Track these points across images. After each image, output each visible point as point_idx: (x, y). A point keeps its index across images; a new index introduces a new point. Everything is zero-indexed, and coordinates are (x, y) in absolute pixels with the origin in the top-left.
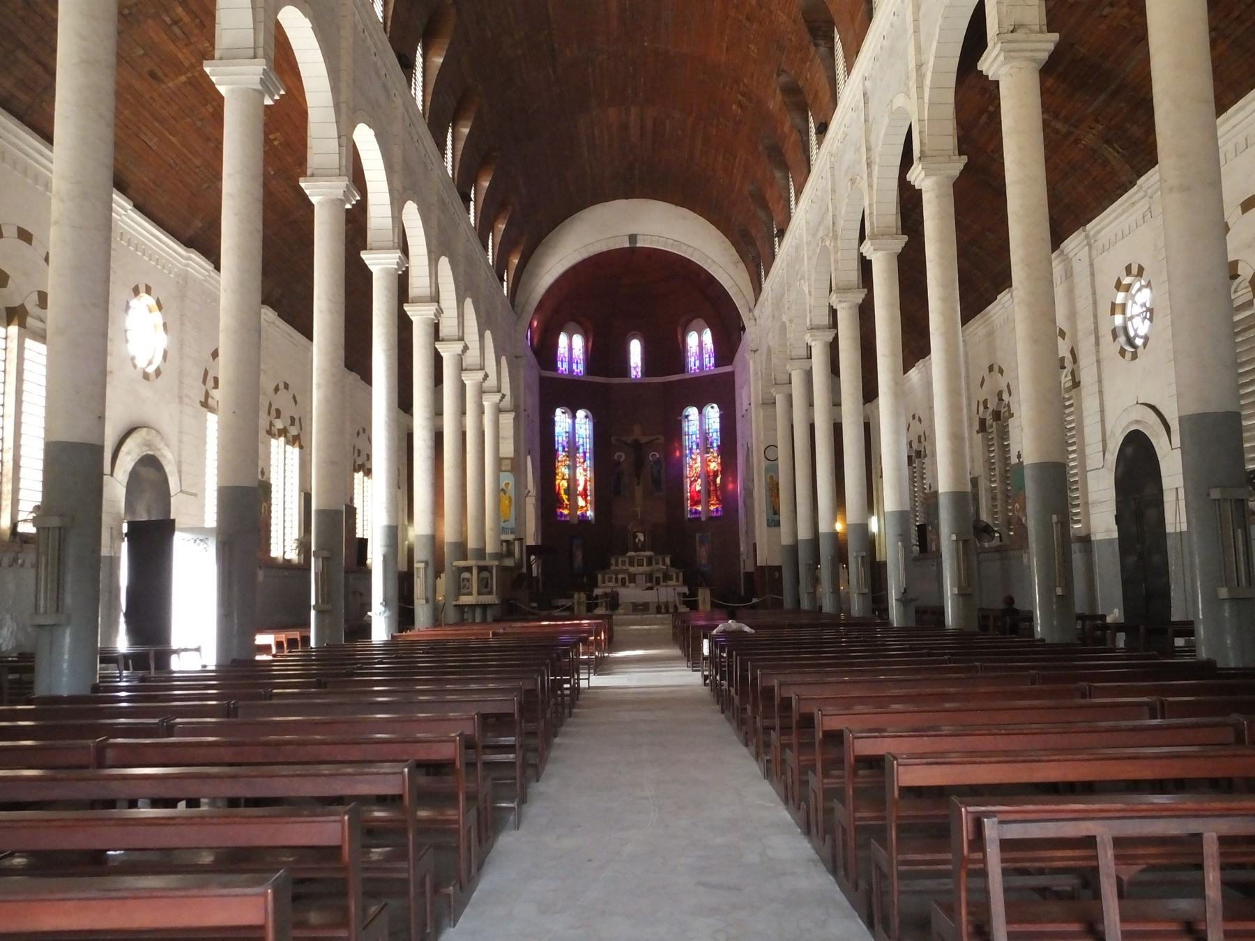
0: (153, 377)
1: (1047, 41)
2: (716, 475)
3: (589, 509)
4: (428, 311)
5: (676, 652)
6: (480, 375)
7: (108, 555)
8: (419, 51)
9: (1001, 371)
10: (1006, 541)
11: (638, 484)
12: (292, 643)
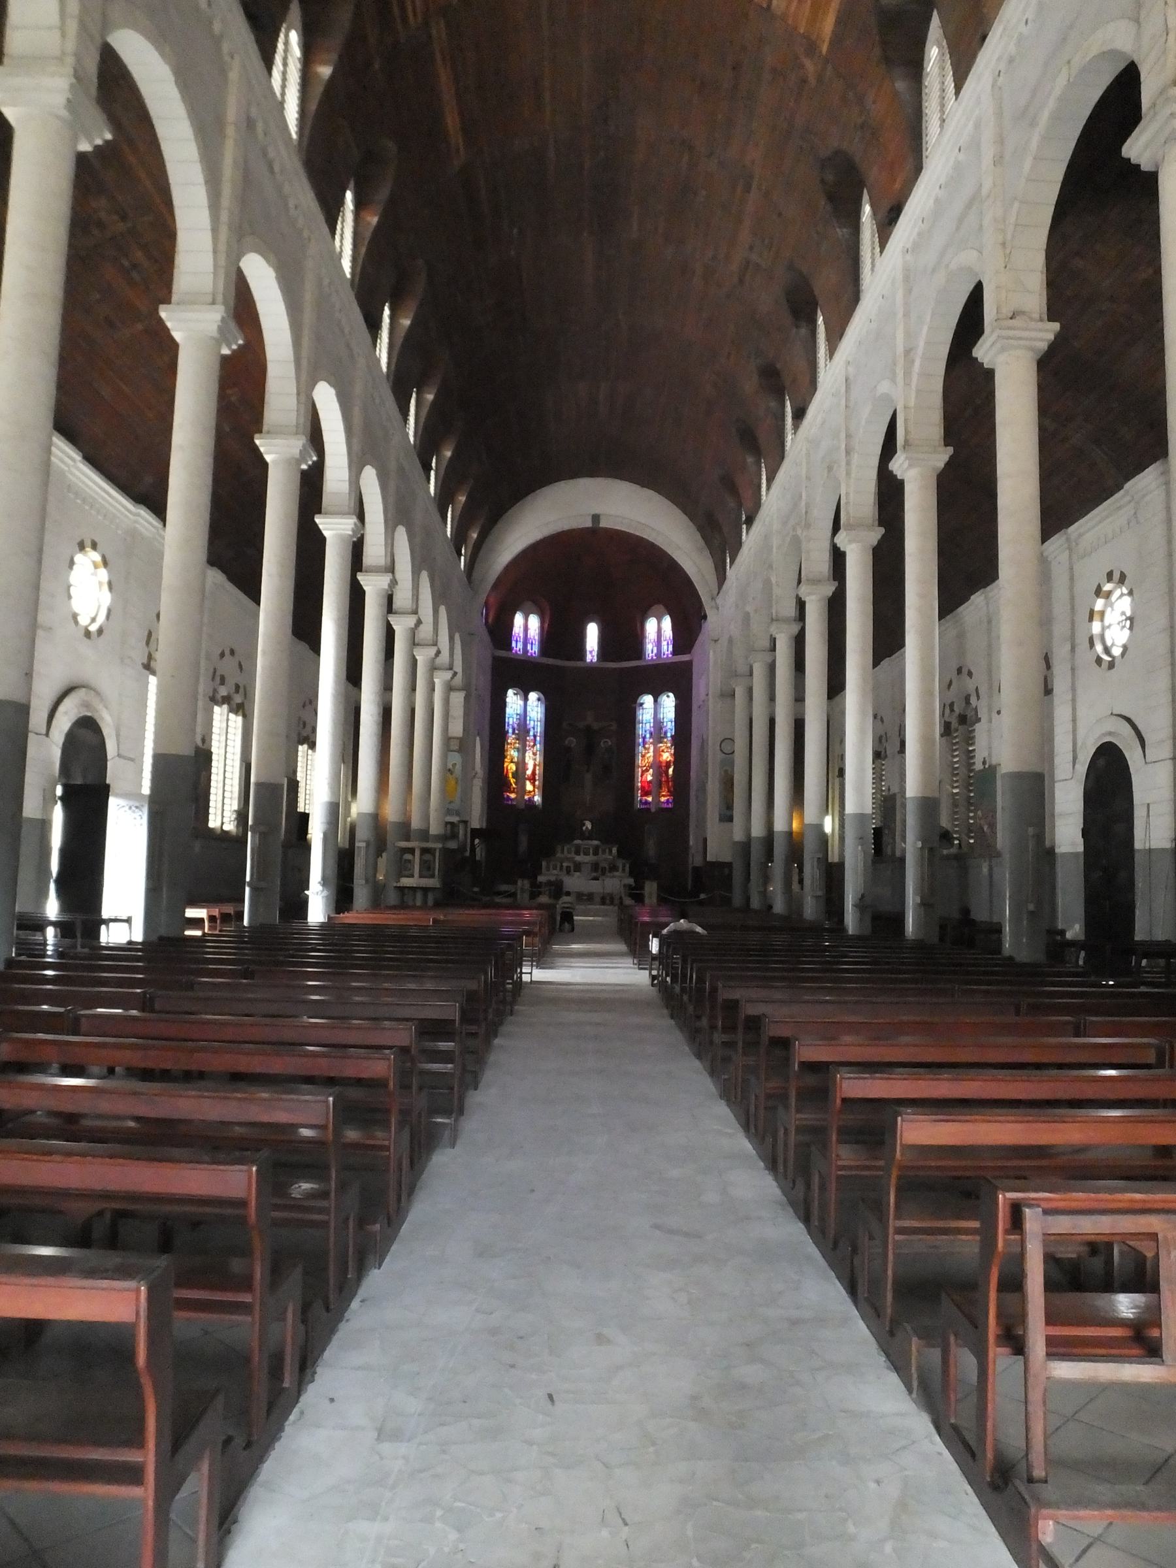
0: (94, 636)
1: (1047, 331)
2: (668, 766)
3: (537, 793)
4: (383, 581)
5: (623, 947)
6: (433, 650)
7: (39, 816)
8: (387, 312)
9: (970, 674)
10: (965, 849)
11: (588, 771)
12: (225, 918)
